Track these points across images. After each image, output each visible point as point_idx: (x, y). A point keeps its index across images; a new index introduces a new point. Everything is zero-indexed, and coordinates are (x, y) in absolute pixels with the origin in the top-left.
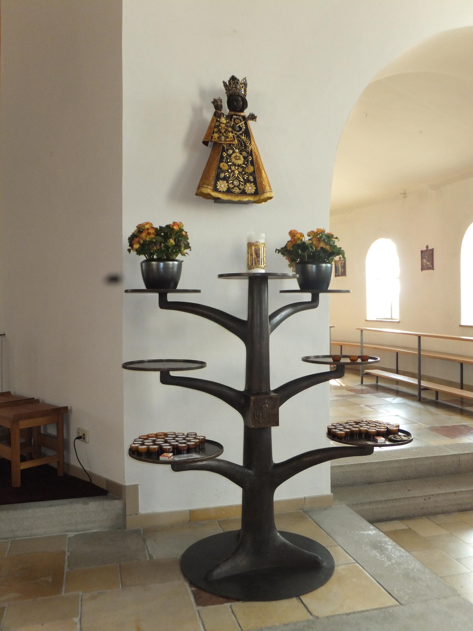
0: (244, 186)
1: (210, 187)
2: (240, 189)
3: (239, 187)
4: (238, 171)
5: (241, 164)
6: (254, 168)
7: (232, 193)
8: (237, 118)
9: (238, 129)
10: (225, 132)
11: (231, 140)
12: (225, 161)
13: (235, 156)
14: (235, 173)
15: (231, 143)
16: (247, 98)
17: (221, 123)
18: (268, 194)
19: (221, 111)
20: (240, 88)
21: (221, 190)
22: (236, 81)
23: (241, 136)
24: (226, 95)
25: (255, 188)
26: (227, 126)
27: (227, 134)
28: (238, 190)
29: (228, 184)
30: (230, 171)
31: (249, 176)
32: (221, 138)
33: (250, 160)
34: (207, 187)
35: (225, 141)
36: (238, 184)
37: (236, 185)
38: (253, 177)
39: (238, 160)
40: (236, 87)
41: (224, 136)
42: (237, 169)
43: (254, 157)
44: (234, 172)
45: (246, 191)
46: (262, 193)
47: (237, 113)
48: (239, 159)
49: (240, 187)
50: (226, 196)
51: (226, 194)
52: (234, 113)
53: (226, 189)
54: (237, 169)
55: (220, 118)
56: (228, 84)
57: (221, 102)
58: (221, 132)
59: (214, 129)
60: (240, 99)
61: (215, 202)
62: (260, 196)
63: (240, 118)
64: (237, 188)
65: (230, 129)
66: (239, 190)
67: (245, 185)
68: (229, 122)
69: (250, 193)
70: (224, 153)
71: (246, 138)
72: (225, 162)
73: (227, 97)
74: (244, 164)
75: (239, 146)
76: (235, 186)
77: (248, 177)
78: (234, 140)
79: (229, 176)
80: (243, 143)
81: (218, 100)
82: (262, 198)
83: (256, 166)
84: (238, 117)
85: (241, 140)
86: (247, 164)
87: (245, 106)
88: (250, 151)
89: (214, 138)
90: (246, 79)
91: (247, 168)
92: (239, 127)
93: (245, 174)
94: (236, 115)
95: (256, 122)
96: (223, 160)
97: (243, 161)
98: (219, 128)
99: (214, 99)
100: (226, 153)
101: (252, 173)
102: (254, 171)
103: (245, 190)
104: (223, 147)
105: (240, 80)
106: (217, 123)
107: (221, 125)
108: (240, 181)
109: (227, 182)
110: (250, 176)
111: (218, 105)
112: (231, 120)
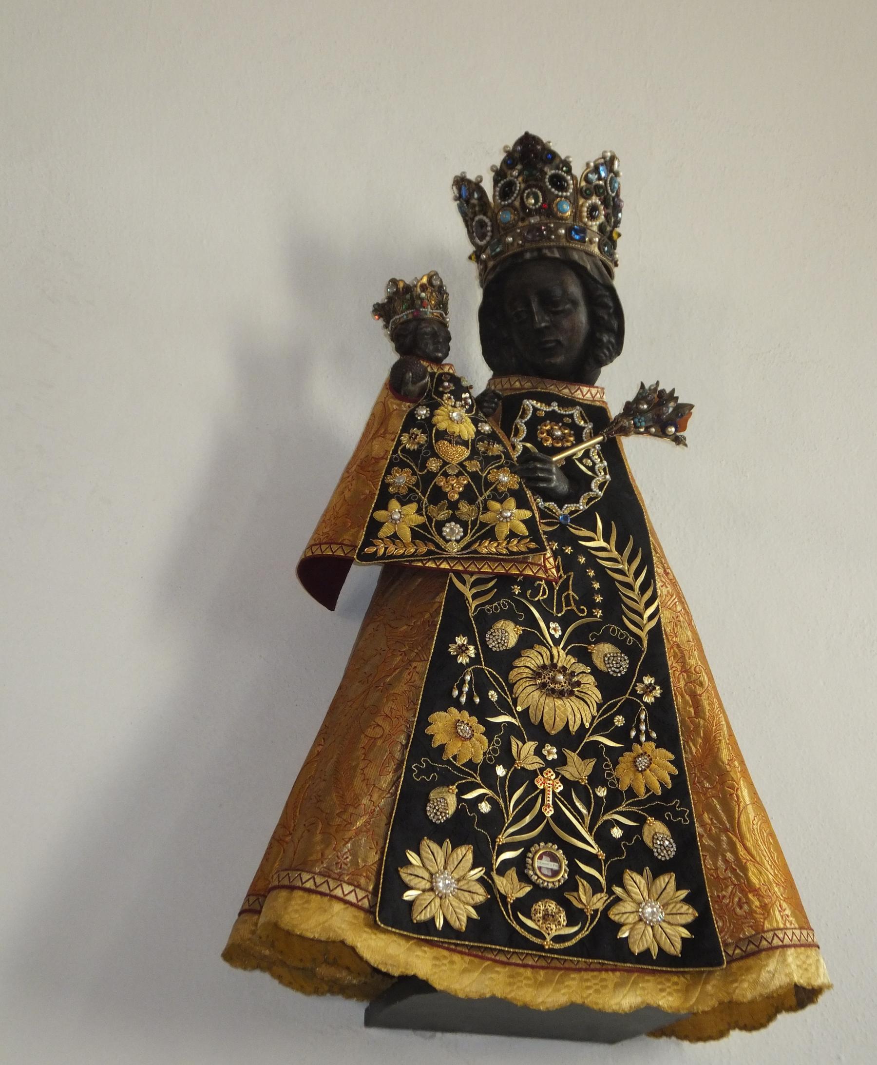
0: (610, 892)
1: (347, 888)
2: (575, 915)
3: (567, 895)
4: (564, 780)
5: (582, 731)
6: (677, 762)
7: (515, 940)
8: (553, 417)
9: (558, 483)
10: (468, 495)
11: (512, 553)
12: (463, 699)
13: (544, 667)
14: (543, 791)
15: (515, 571)
16: (620, 282)
17: (443, 435)
18: (790, 959)
19: (438, 361)
20: (574, 220)
21: (433, 920)
22: (550, 172)
23: (584, 533)
24: (473, 269)
25: (689, 914)
26: (487, 460)
27: (486, 509)
28: (560, 927)
29: (488, 873)
30: (500, 771)
31: (642, 821)
32: (440, 532)
33: (649, 699)
34: (324, 889)
35: (470, 554)
36: (564, 875)
37: (552, 883)
38: (668, 824)
39: (561, 694)
40: (548, 211)
41: (464, 525)
42: (552, 764)
43: (678, 682)
44: (533, 787)
45: (624, 934)
46: (747, 956)
47: (552, 388)
48: (571, 693)
49: (575, 903)
50: (465, 971)
51: (470, 952)
52: (528, 385)
53: (474, 914)
54: (552, 764)
55: (434, 406)
56: (488, 186)
57: (443, 305)
58: (438, 496)
59: (388, 472)
60: (575, 290)
61: (369, 1021)
62: (731, 978)
63: (571, 416)
64: (552, 906)
65: (506, 478)
66: (570, 924)
67: (618, 890)
68: (493, 437)
69: (655, 952)
70: (461, 640)
71: (620, 549)
72: (470, 707)
73: (477, 282)
74: (604, 726)
75: (568, 604)
76: (539, 893)
77: (639, 830)
78: (531, 551)
79: (497, 812)
80: (596, 578)
81: (424, 288)
82: (749, 996)
83: (692, 750)
84: (555, 406)
85: (582, 560)
86: (626, 729)
87: (605, 338)
88: (643, 635)
89: (386, 531)
90: (616, 163)
91: (628, 756)
92: (569, 467)
93: (614, 799)
94: (547, 399)
95: (679, 449)
96: (456, 693)
97: (599, 706)
98: (423, 467)
99: (394, 282)
100: (472, 641)
101: (667, 795)
102: (679, 780)
103: (619, 926)
104: (456, 599)
105: (578, 170)
106: (413, 437)
107: (443, 446)
108: (572, 853)
109: (481, 859)
110: (650, 819)
111: (419, 319)
112: (508, 427)
